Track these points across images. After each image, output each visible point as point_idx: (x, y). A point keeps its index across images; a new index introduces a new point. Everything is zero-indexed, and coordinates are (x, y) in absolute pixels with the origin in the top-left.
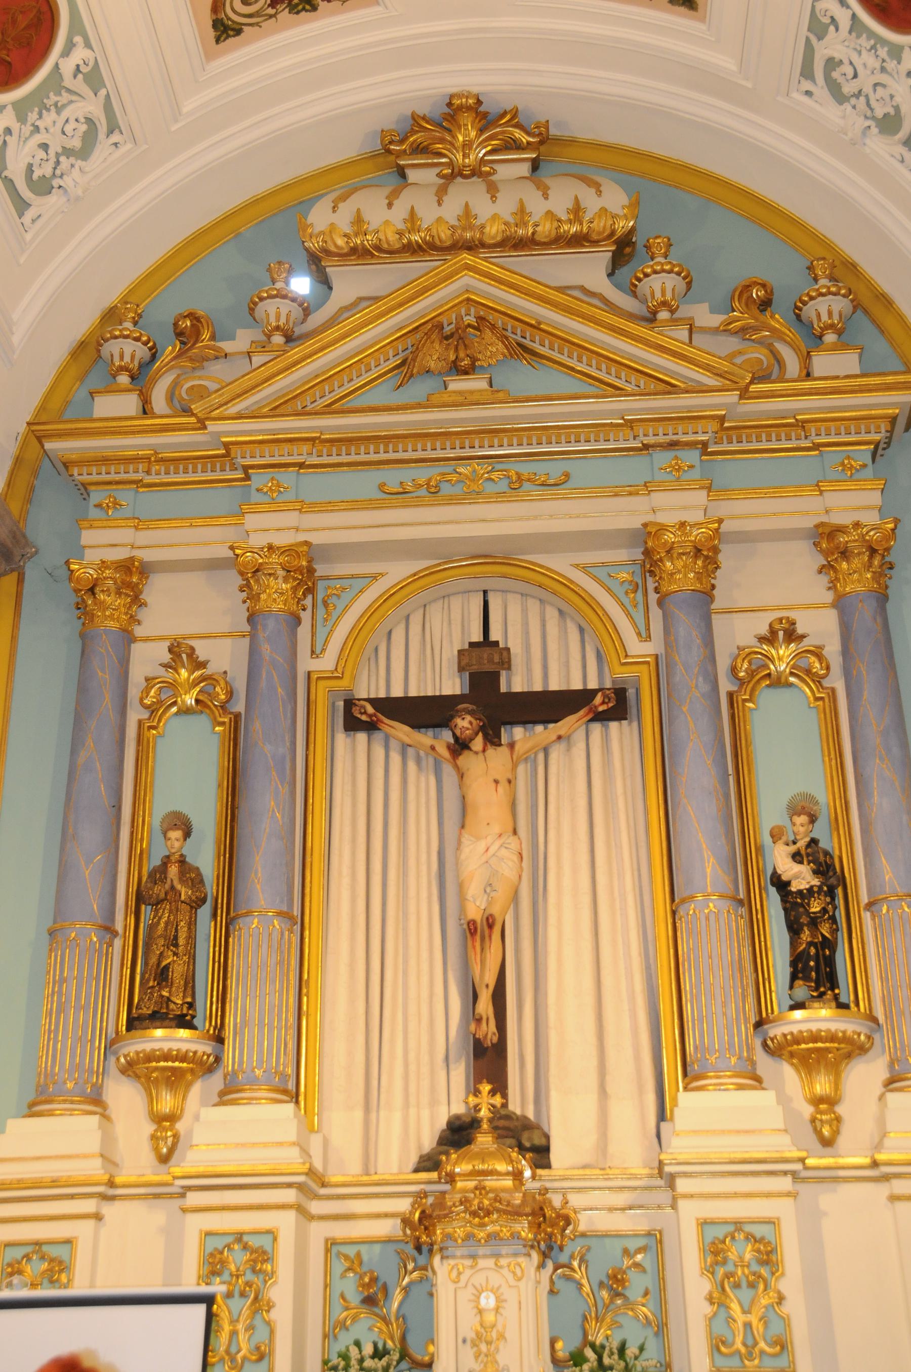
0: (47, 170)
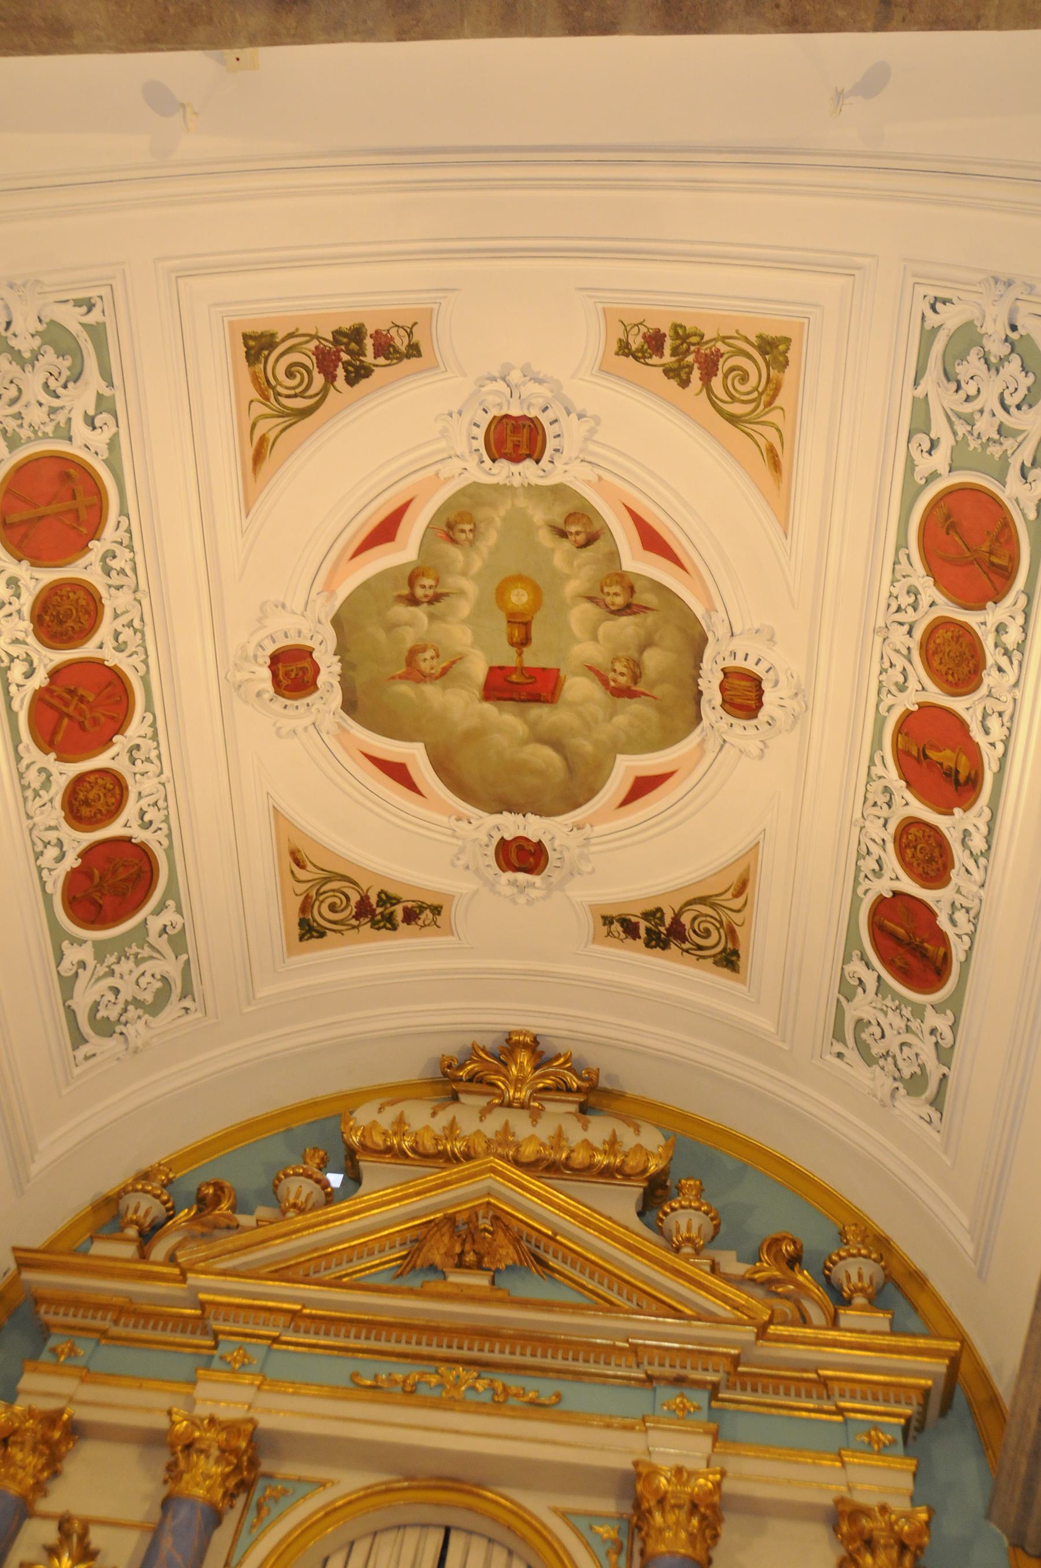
0: (113, 1014)
